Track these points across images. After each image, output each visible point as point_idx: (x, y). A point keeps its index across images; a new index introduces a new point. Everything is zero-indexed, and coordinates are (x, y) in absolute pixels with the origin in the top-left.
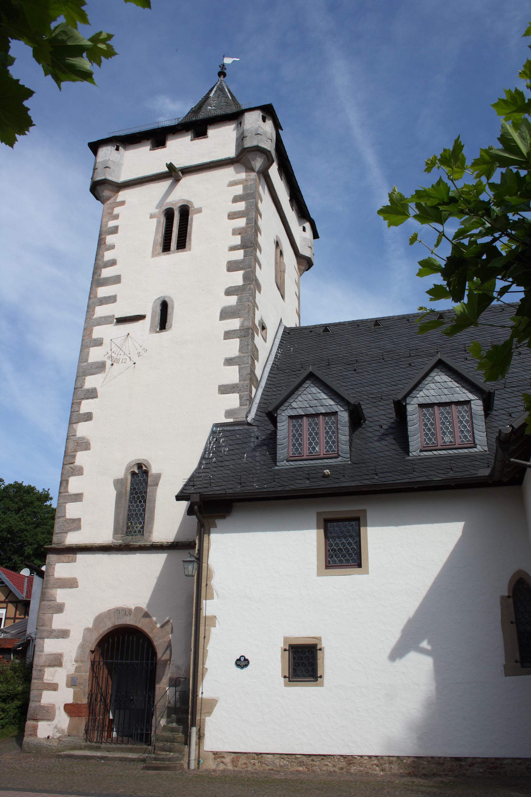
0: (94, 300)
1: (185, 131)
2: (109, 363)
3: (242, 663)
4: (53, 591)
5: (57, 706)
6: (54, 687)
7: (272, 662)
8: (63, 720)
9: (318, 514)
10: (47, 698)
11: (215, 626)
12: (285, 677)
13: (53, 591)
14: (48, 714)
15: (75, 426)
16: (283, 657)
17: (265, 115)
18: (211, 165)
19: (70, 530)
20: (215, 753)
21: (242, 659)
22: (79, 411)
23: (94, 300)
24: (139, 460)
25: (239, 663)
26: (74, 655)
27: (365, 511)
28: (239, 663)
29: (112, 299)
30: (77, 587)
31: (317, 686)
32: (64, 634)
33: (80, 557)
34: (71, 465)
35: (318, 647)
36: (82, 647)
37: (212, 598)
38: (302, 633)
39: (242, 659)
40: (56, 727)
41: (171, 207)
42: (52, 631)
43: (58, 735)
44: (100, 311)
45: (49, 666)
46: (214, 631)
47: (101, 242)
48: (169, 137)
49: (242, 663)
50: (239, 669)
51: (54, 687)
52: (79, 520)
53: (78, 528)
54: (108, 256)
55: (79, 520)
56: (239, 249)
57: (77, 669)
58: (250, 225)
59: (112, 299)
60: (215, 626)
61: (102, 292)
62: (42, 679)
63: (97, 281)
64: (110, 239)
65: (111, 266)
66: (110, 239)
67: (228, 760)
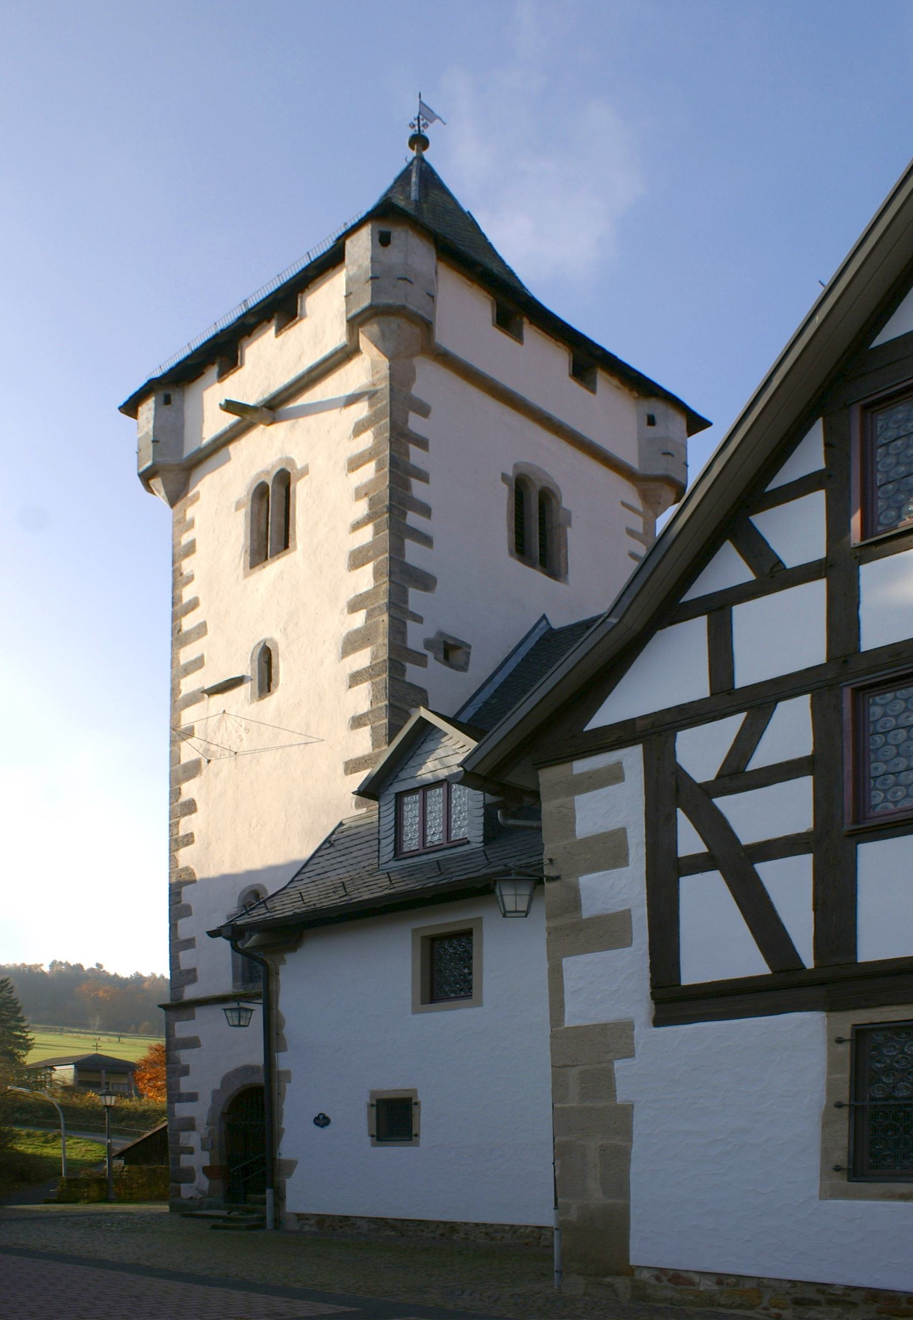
0: (180, 671)
1: (265, 323)
2: (204, 762)
3: (322, 1121)
4: (177, 1053)
5: (196, 1169)
6: (191, 1151)
7: (355, 1120)
8: (202, 1182)
9: (414, 931)
10: (186, 1161)
11: (290, 1082)
12: (372, 1136)
13: (177, 1053)
14: (188, 1175)
15: (175, 854)
16: (369, 1114)
17: (385, 228)
18: (313, 374)
19: (186, 984)
20: (298, 1215)
21: (321, 1117)
22: (178, 834)
23: (180, 671)
24: (252, 886)
25: (317, 1121)
26: (205, 1119)
27: (480, 919)
28: (317, 1121)
29: (199, 663)
30: (200, 1046)
31: (411, 1146)
32: (192, 1097)
33: (198, 1011)
34: (179, 905)
35: (414, 1101)
36: (212, 1109)
37: (285, 1050)
38: (392, 1083)
39: (321, 1117)
40: (197, 1189)
41: (259, 481)
42: (181, 1095)
43: (200, 1196)
44: (188, 685)
45: (183, 1130)
46: (288, 1086)
47: (177, 573)
48: (244, 342)
49: (322, 1121)
50: (318, 1128)
51: (191, 1151)
52: (194, 970)
53: (194, 980)
54: (187, 594)
55: (194, 970)
56: (366, 524)
57: (211, 1133)
58: (381, 473)
59: (199, 663)
60: (290, 1082)
61: (187, 654)
62: (178, 1143)
63: (179, 639)
64: (187, 566)
65: (193, 609)
66: (187, 566)
67: (313, 1222)
